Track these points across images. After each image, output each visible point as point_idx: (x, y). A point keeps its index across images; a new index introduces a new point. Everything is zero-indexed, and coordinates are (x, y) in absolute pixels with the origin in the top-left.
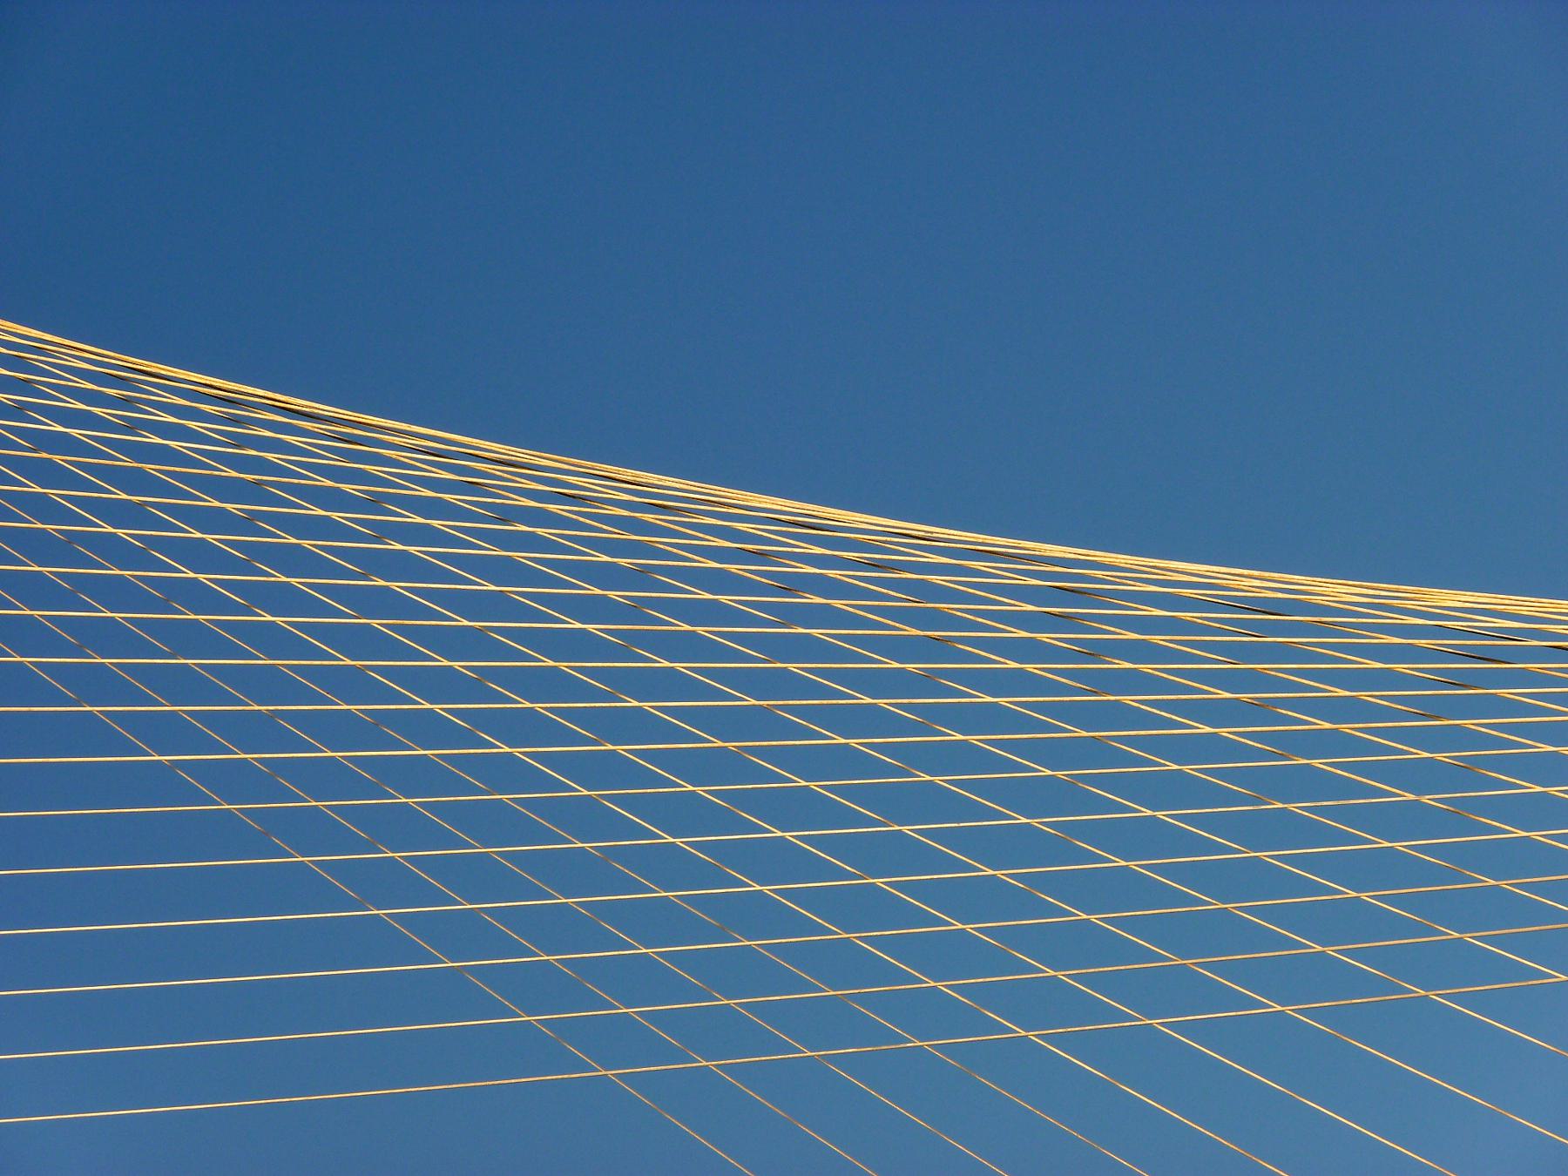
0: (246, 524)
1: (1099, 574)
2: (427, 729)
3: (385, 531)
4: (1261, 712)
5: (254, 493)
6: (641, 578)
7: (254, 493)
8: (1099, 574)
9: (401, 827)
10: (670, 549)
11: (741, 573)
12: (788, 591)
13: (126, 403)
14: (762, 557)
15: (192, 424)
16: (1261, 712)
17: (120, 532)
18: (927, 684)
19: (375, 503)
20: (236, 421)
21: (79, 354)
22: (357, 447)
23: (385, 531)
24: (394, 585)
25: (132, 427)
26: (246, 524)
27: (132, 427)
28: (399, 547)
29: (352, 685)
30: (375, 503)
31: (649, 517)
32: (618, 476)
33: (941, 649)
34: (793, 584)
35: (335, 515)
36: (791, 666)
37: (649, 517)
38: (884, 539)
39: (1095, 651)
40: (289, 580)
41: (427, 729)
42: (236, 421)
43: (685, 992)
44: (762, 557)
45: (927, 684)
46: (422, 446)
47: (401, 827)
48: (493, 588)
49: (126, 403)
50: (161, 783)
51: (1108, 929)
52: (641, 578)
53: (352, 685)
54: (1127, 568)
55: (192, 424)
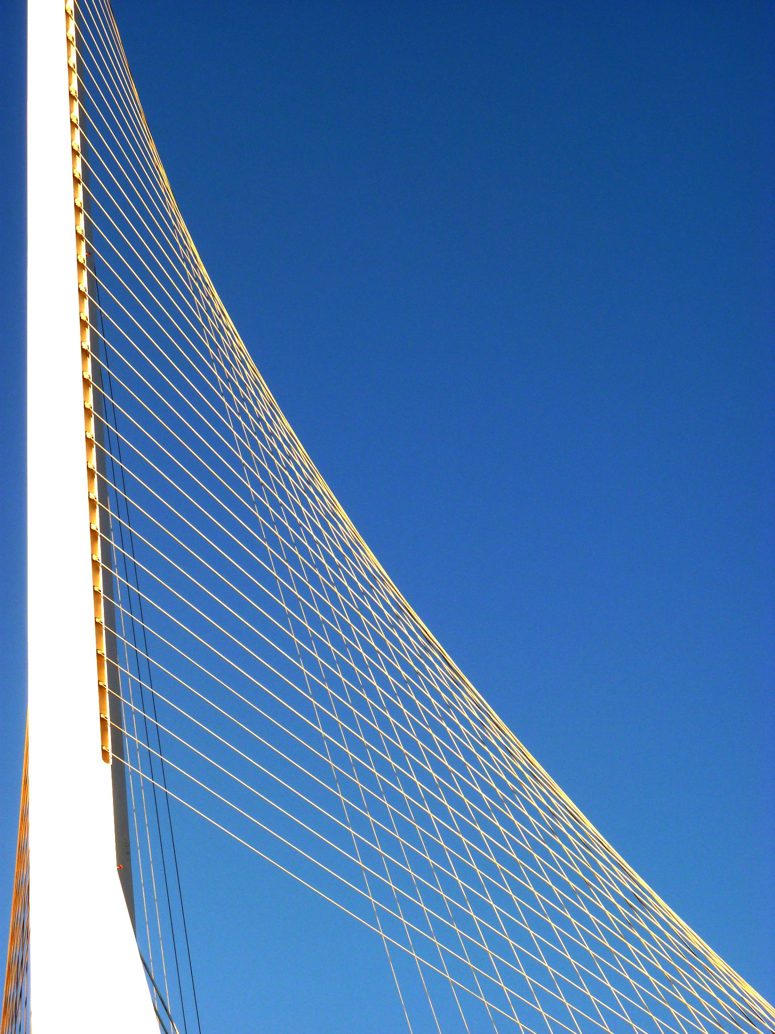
0: (405, 683)
1: (651, 900)
2: (410, 787)
3: (444, 717)
4: (669, 983)
5: (415, 675)
6: (511, 793)
7: (415, 675)
8: (651, 900)
9: (379, 811)
10: (601, 882)
11: (645, 944)
12: (553, 833)
13: (397, 617)
14: (553, 815)
15: (411, 638)
16: (669, 983)
17: (466, 800)
18: (573, 893)
19: (448, 707)
20: (426, 649)
21: (393, 590)
22: (457, 686)
23: (444, 717)
24: (434, 736)
25: (393, 626)
26: (405, 683)
27: (393, 626)
28: (403, 673)
29: (398, 756)
30: (448, 707)
31: (527, 776)
32: (528, 757)
33: (586, 887)
34: (556, 831)
35: (433, 700)
36: (535, 855)
37: (527, 776)
38: (596, 840)
39: (633, 924)
40: (464, 798)
41: (410, 787)
42: (426, 649)
43: (426, 929)
44: (553, 815)
45: (573, 893)
46: (453, 676)
47: (379, 811)
48: (463, 759)
49: (397, 617)
50: (316, 740)
51: (138, 326)
52: (511, 793)
53: (398, 756)
54: (715, 968)
55: (411, 638)
